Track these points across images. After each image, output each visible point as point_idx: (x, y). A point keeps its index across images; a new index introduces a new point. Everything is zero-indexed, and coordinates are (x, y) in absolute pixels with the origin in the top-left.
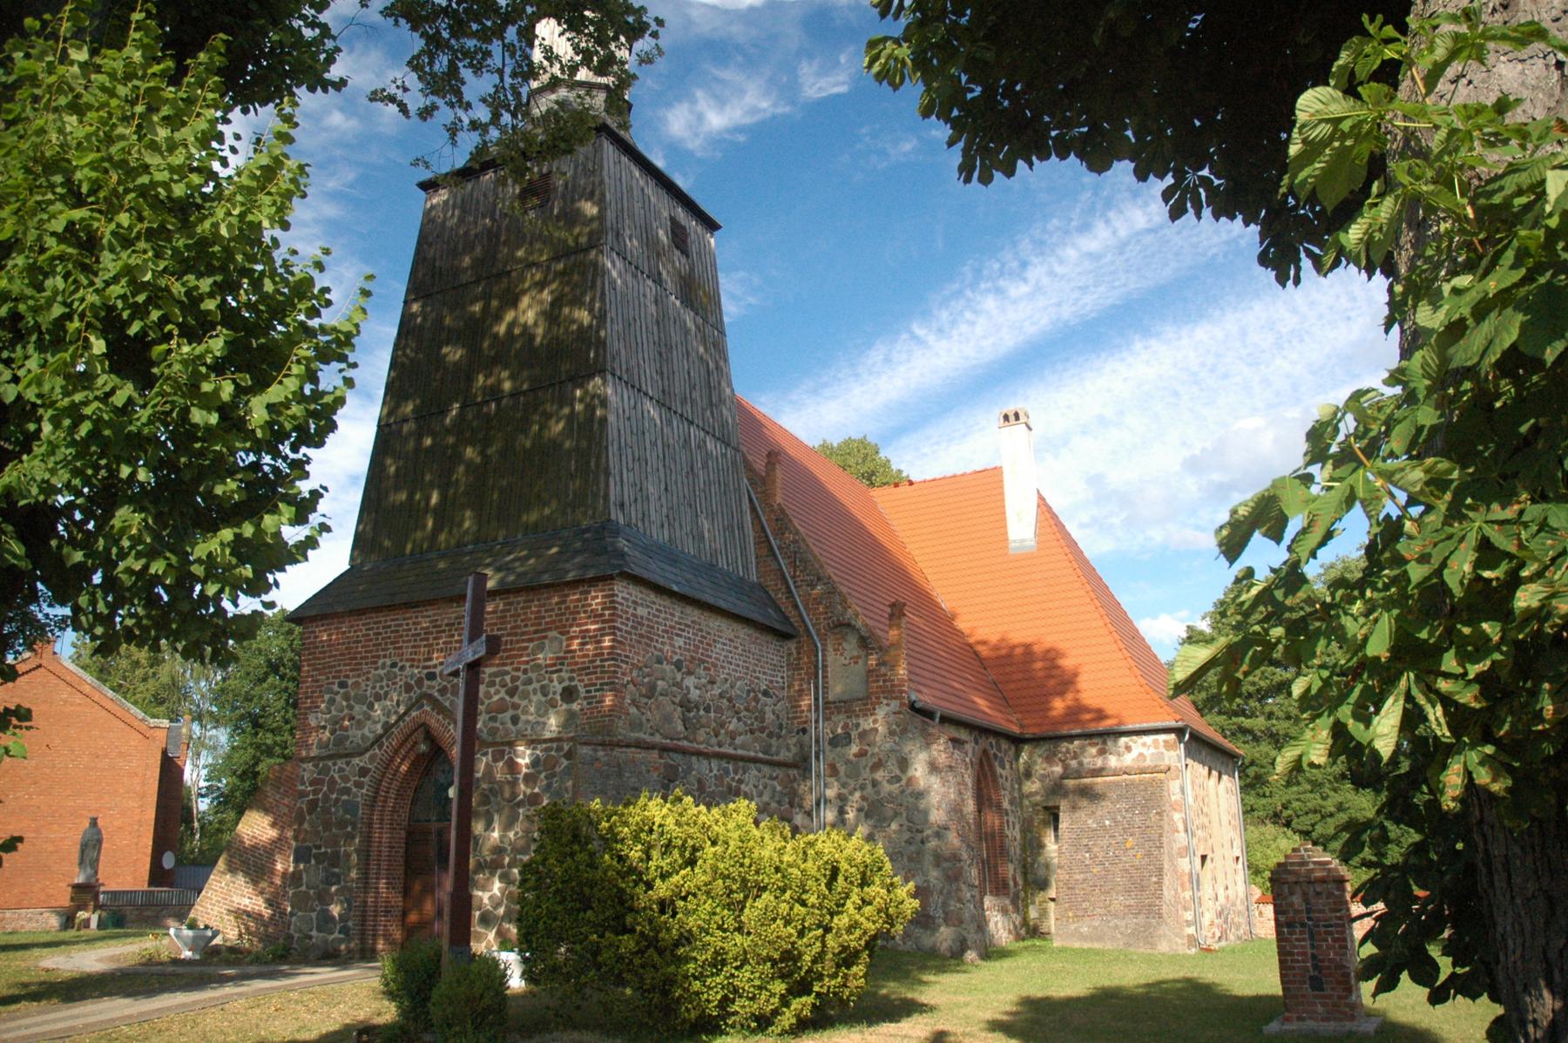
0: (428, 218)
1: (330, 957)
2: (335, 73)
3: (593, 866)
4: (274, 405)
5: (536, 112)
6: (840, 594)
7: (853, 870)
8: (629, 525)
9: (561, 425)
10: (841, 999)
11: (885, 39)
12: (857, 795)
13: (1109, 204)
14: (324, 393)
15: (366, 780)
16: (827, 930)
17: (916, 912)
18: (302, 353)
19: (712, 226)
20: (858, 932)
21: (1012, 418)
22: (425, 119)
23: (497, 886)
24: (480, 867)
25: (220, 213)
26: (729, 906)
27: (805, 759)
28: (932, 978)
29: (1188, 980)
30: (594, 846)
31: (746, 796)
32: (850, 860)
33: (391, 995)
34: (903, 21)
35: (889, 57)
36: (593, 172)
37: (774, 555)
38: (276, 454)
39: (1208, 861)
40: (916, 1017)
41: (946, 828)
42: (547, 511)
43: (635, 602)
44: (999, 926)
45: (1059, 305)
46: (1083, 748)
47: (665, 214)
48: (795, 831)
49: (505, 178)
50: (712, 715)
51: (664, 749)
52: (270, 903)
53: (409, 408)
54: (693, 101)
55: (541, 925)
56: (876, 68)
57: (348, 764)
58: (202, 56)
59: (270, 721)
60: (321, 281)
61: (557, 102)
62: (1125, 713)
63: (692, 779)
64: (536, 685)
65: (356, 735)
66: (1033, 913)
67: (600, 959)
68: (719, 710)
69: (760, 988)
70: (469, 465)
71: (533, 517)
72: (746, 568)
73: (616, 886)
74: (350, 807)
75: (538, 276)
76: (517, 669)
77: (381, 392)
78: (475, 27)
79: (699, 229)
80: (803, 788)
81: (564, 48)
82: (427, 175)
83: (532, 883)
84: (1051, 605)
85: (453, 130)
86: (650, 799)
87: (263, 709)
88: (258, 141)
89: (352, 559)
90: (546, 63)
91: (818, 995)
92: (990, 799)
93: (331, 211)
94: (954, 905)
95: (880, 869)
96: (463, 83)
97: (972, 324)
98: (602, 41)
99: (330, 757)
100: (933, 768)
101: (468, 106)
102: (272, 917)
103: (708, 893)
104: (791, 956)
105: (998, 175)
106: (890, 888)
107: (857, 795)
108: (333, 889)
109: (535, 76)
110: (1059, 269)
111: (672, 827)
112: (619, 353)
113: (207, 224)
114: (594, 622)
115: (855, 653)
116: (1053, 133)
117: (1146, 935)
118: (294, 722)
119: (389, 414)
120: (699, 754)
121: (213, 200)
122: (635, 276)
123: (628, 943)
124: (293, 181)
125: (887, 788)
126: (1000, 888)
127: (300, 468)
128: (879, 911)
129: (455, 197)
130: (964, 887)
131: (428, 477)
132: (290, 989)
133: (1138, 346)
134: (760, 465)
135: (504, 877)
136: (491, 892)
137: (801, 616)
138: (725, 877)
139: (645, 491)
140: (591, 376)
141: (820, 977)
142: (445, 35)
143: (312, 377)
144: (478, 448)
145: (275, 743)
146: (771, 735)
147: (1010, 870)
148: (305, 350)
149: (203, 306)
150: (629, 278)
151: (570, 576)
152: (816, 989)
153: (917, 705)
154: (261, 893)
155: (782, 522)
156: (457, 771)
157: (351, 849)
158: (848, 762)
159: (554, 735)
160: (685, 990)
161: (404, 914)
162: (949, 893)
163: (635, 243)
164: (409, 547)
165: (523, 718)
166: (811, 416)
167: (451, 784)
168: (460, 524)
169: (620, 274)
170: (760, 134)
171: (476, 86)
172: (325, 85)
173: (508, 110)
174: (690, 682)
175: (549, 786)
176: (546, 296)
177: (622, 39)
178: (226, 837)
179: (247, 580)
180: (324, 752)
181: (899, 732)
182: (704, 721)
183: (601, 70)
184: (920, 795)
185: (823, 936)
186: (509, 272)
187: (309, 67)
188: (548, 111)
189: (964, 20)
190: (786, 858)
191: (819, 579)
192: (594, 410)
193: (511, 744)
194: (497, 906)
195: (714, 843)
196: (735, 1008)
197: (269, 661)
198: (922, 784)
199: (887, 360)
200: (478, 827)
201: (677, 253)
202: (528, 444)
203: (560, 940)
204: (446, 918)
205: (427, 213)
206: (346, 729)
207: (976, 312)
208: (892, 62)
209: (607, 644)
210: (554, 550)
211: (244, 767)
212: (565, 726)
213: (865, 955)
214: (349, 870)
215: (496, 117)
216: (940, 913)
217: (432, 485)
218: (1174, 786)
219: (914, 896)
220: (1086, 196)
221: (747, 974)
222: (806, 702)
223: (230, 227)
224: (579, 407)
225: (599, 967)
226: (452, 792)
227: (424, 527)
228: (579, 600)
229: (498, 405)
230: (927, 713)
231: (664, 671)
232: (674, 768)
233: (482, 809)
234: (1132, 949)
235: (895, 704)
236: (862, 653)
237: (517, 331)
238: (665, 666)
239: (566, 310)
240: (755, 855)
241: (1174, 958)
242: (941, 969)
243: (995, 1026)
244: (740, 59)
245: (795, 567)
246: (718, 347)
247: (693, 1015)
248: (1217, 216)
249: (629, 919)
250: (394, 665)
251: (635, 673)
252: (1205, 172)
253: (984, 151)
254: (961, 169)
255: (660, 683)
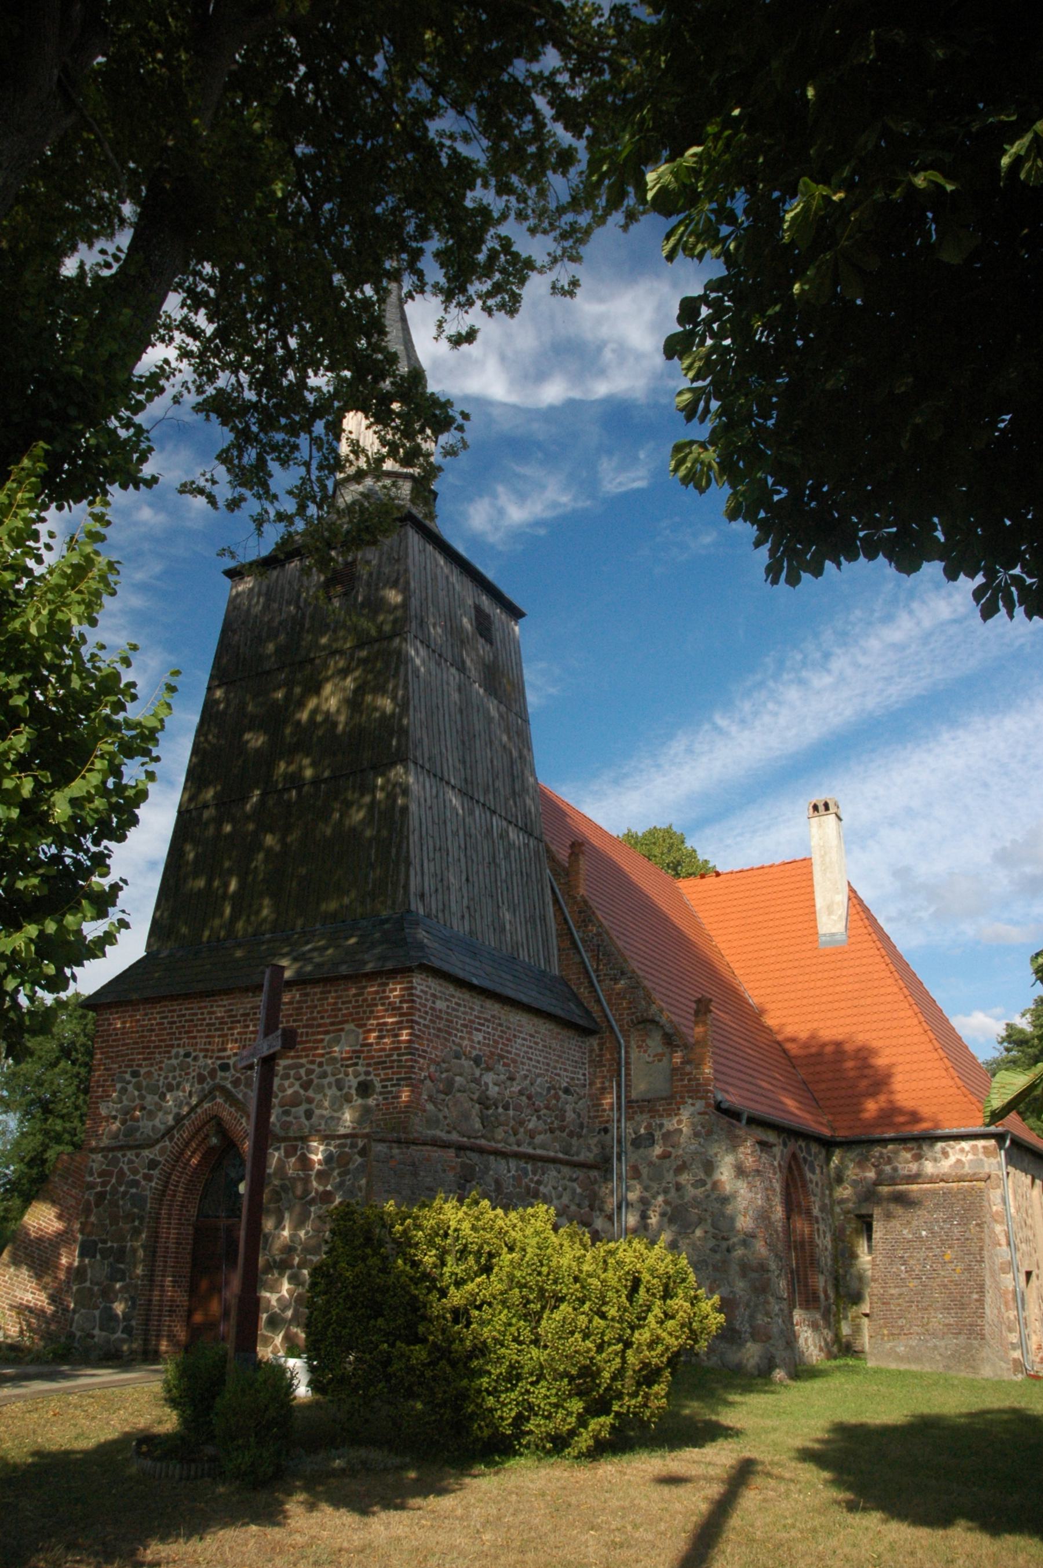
0: (233, 603)
1: (112, 1358)
2: (147, 470)
3: (385, 1270)
4: (77, 799)
5: (341, 503)
6: (644, 988)
7: (655, 1281)
8: (429, 916)
9: (361, 815)
10: (641, 1420)
11: (691, 443)
12: (660, 1199)
13: (911, 595)
14: (126, 787)
15: (155, 1173)
16: (628, 1344)
17: (721, 1327)
18: (106, 748)
19: (516, 614)
20: (660, 1348)
21: (821, 808)
22: (232, 511)
23: (286, 1287)
24: (269, 1268)
25: (31, 613)
26: (525, 1317)
27: (608, 1160)
28: (737, 1398)
29: (1014, 1411)
30: (387, 1250)
31: (547, 1200)
32: (652, 1271)
33: (173, 1402)
34: (709, 425)
35: (696, 461)
36: (398, 560)
37: (577, 948)
38: (78, 847)
39: (1033, 1277)
40: (721, 1442)
41: (754, 1236)
42: (346, 901)
43: (434, 995)
44: (810, 1342)
45: (864, 695)
46: (896, 1152)
47: (470, 602)
48: (596, 1237)
49: (310, 568)
50: (511, 1112)
51: (460, 1148)
52: (53, 1299)
53: (210, 794)
54: (495, 496)
55: (330, 1333)
56: (682, 471)
57: (137, 1155)
58: (26, 462)
59: (60, 1107)
60: (127, 676)
61: (362, 494)
62: (940, 1117)
63: (489, 1180)
64: (331, 1079)
65: (146, 1127)
66: (845, 1329)
67: (390, 1370)
68: (518, 1108)
69: (557, 1406)
70: (269, 851)
71: (332, 906)
72: (548, 961)
73: (408, 1293)
74: (138, 1201)
75: (342, 664)
76: (312, 1062)
77: (182, 779)
78: (283, 421)
79: (503, 616)
80: (604, 1191)
81: (370, 442)
82: (231, 564)
83: (321, 1287)
84: (862, 1002)
85: (259, 521)
86: (446, 1201)
87: (54, 1094)
88: (72, 539)
89: (149, 945)
90: (352, 457)
91: (618, 1415)
92: (799, 1205)
93: (137, 601)
94: (761, 1320)
95: (683, 1280)
96: (271, 476)
97: (776, 714)
98: (408, 434)
99: (120, 1148)
100: (740, 1171)
101: (275, 497)
102: (55, 1314)
103: (503, 1302)
104: (589, 1372)
105: (806, 576)
106: (694, 1301)
107: (660, 1199)
108: (118, 1286)
109: (341, 468)
110: (863, 660)
111: (468, 1232)
112: (421, 741)
113: (17, 624)
114: (394, 1015)
115: (660, 1050)
116: (861, 534)
117: (967, 1358)
118: (85, 1109)
119: (191, 799)
120: (497, 1153)
121: (24, 597)
122: (439, 664)
123: (419, 1353)
124: (103, 579)
125: (691, 1192)
126: (810, 1301)
127: (100, 861)
128: (683, 1326)
129: (260, 584)
130: (771, 1300)
131: (227, 864)
132: (68, 1392)
133: (945, 736)
134: (563, 855)
135: (294, 1279)
136: (280, 1293)
137: (603, 1010)
138: (522, 1286)
139: (446, 885)
140: (393, 764)
141: (619, 1396)
142: (255, 429)
143: (116, 771)
144: (278, 837)
145: (65, 1130)
146: (571, 1134)
147: (821, 1282)
148: (107, 746)
149: (11, 702)
150: (433, 666)
151: (369, 967)
152: (615, 1408)
153: (724, 1106)
154: (45, 1288)
155: (586, 914)
156: (249, 1165)
157: (138, 1245)
158: (651, 1164)
159: (348, 1131)
160: (477, 1405)
161: (190, 1313)
162: (756, 1306)
163: (439, 630)
164: (207, 933)
165: (318, 1112)
166: (615, 807)
167: (241, 1180)
168: (258, 912)
169: (423, 662)
170: (561, 529)
171: (283, 478)
172: (137, 483)
173: (314, 502)
174: (489, 1078)
175: (341, 1185)
176: (349, 683)
177: (429, 432)
178: (12, 1226)
179: (47, 977)
180: (114, 1143)
181: (704, 1133)
182: (502, 1118)
183: (406, 462)
184: (725, 1200)
185: (623, 1351)
186: (314, 659)
187: (123, 465)
188: (354, 503)
189: (770, 423)
190: (585, 1268)
191: (623, 973)
192: (395, 801)
193: (305, 1139)
194: (284, 1309)
195: (511, 1249)
196: (530, 1426)
197: (61, 1045)
198: (728, 1188)
199: (690, 751)
200: (269, 1225)
201: (481, 641)
202: (329, 831)
203: (349, 1349)
204: (233, 1321)
205: (232, 601)
206: (137, 1120)
207: (779, 703)
208: (698, 466)
209: (404, 1038)
210: (353, 941)
211: (33, 1154)
212: (359, 1122)
213: (667, 1373)
214: (135, 1267)
215: (302, 508)
216: (747, 1327)
217: (230, 872)
218: (995, 1195)
219: (720, 1310)
220: (890, 586)
221: (543, 1391)
222: (609, 1100)
223: (39, 625)
224: (380, 795)
225: (388, 1378)
226: (242, 1188)
227: (222, 915)
228: (377, 992)
229: (299, 794)
230: (732, 1114)
231: (462, 1066)
232: (472, 1168)
233: (272, 1206)
234: (952, 1373)
235: (700, 1105)
236: (667, 1050)
237: (319, 718)
238: (463, 1061)
239: (369, 698)
240: (554, 1264)
241: (998, 1385)
242: (747, 1389)
243: (806, 1455)
244: (540, 455)
245: (598, 960)
246: (521, 735)
247: (487, 1432)
248: (1029, 615)
249: (421, 1329)
250: (187, 1055)
251: (432, 1069)
252: (1017, 571)
253: (792, 553)
254: (769, 569)
255: (458, 1078)
